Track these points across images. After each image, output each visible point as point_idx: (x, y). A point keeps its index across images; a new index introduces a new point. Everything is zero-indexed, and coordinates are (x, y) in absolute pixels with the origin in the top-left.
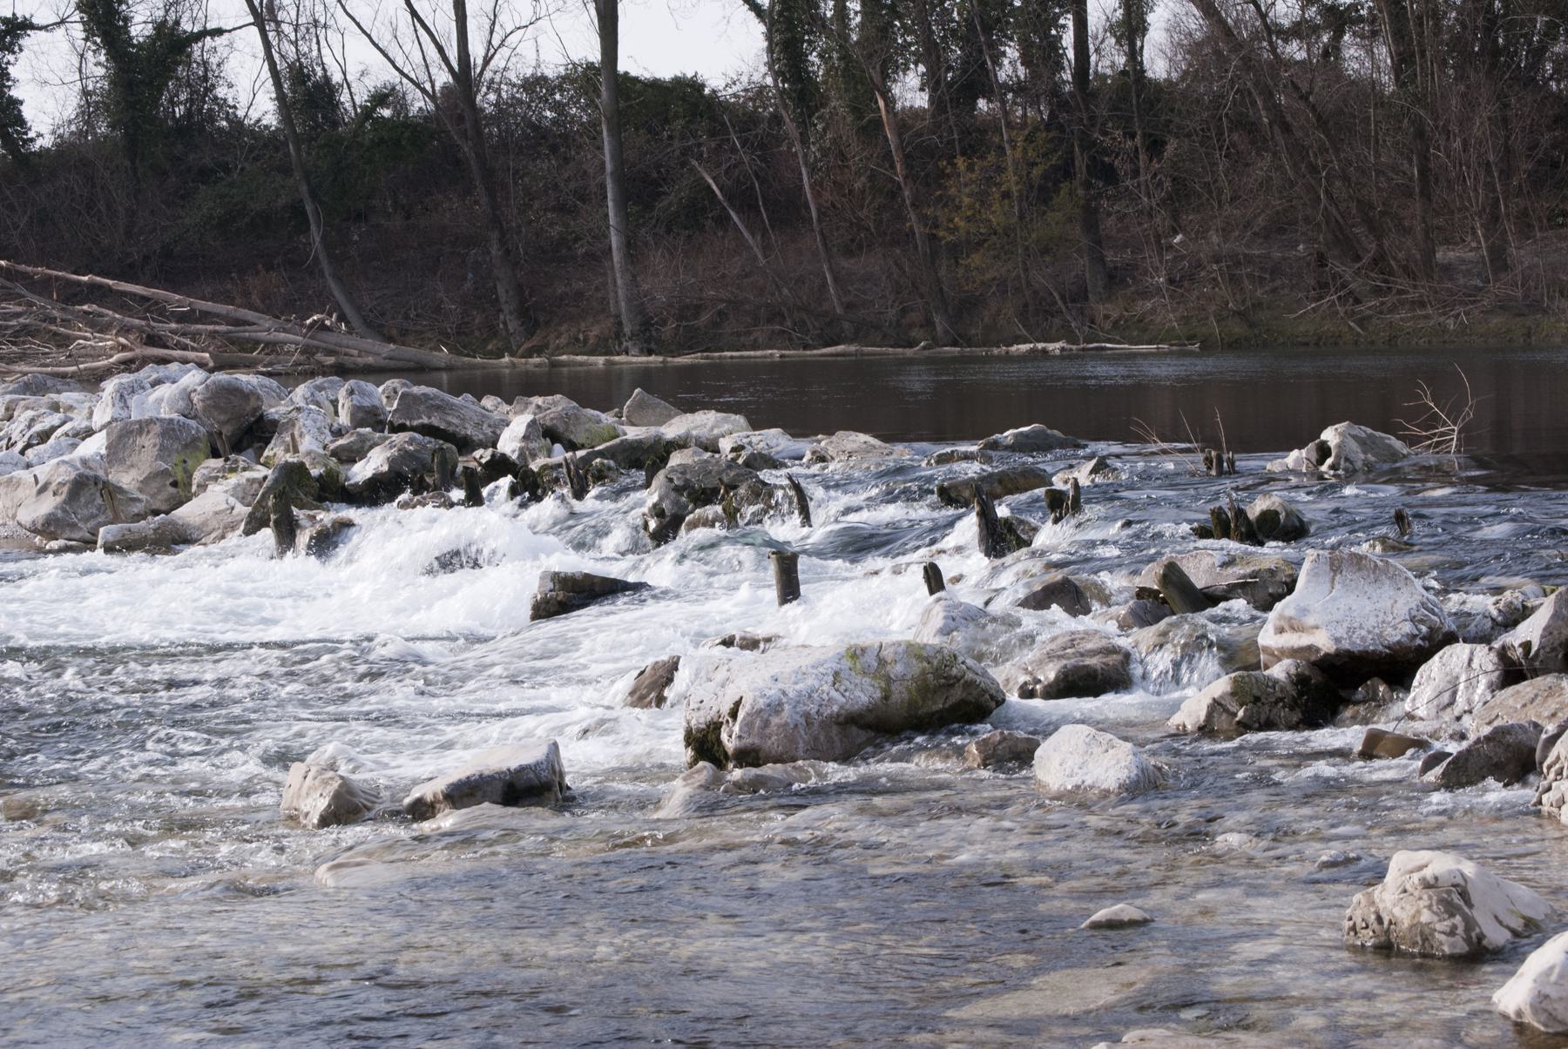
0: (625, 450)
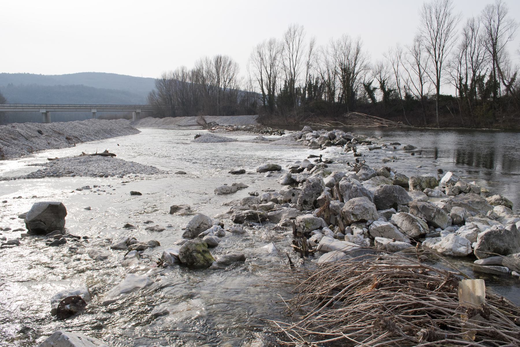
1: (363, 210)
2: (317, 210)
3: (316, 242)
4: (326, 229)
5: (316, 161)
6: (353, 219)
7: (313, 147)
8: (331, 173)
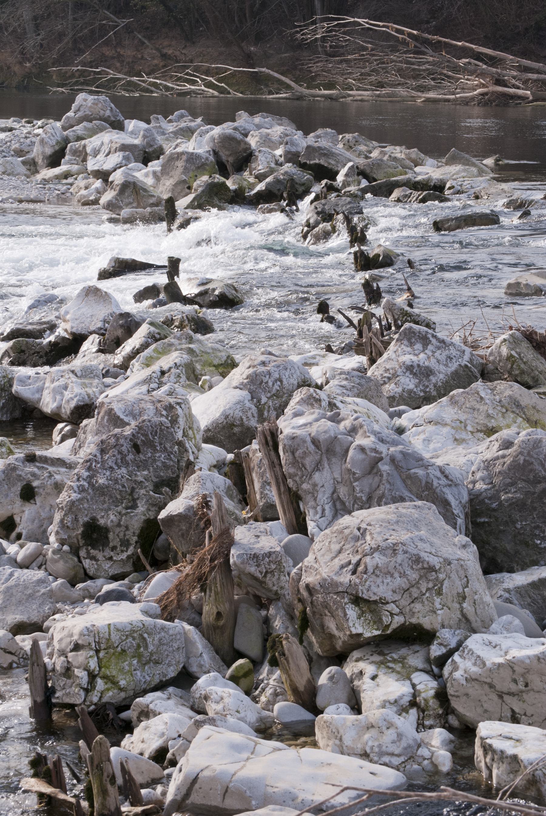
0: (387, 186)
1: (414, 576)
2: (161, 581)
3: (160, 756)
4: (215, 686)
5: (150, 292)
6: (358, 625)
7: (125, 212)
8: (230, 365)
